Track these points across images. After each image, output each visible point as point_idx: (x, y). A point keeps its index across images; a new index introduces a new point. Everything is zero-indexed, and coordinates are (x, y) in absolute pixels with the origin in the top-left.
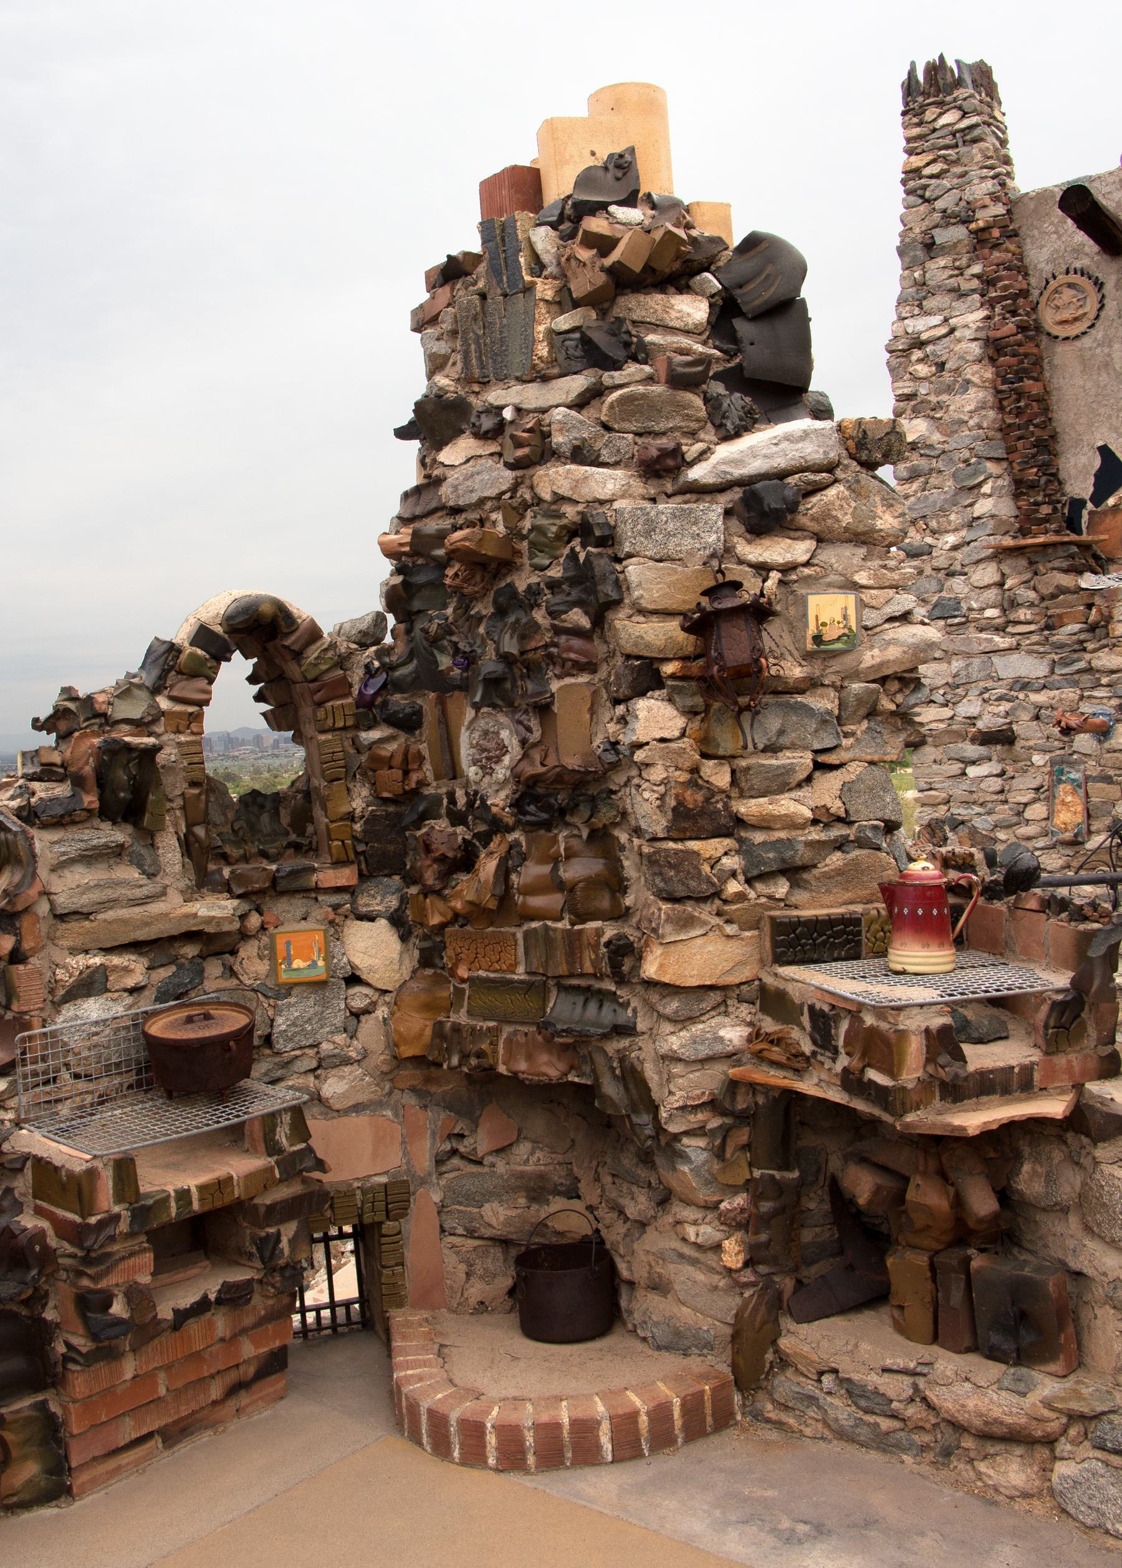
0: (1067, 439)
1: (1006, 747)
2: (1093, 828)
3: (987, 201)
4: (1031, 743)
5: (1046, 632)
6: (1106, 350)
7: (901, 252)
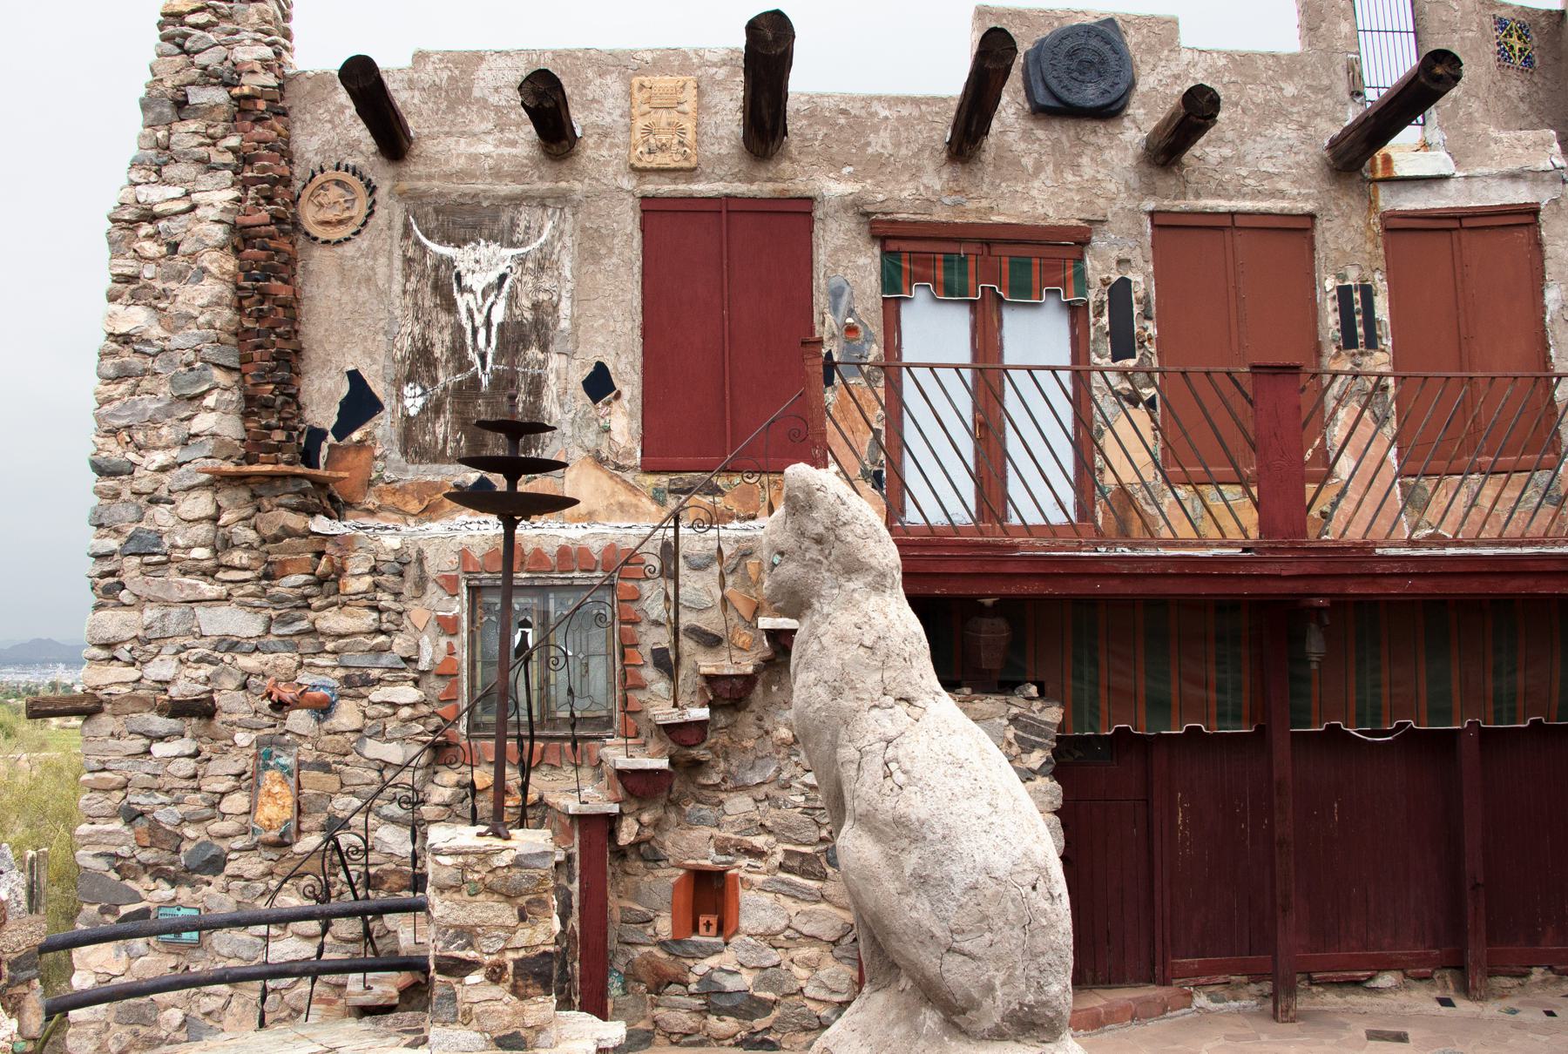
0: (313, 357)
1: (203, 722)
2: (304, 827)
3: (257, 67)
4: (235, 718)
5: (264, 582)
6: (371, 263)
7: (145, 106)
